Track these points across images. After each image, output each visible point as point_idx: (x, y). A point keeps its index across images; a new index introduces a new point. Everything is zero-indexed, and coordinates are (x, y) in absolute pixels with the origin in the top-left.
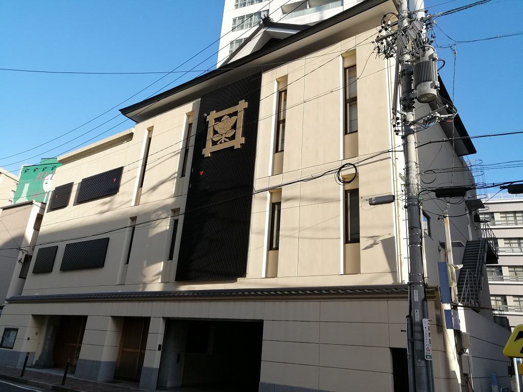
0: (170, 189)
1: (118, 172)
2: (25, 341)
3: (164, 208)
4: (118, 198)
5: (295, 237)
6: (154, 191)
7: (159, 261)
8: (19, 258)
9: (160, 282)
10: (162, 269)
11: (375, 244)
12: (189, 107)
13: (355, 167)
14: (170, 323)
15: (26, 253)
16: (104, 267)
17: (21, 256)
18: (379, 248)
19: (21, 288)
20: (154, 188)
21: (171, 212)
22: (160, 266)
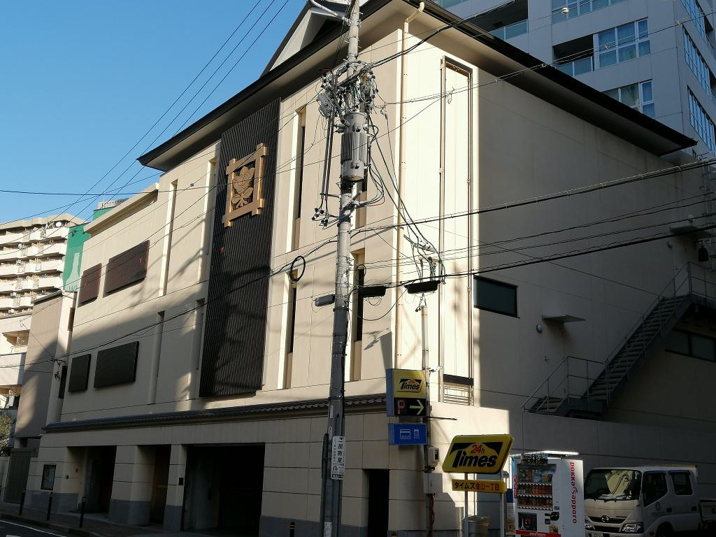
0: (196, 272)
1: (143, 249)
2: (64, 480)
3: (189, 300)
4: (148, 284)
5: (307, 335)
6: (182, 274)
7: (186, 373)
8: (55, 372)
9: (188, 398)
10: (189, 382)
11: (375, 341)
12: (211, 152)
13: (303, 258)
14: (193, 452)
15: (63, 364)
16: (136, 382)
17: (57, 369)
18: (378, 346)
19: (59, 413)
20: (182, 270)
21: (196, 305)
22: (188, 379)
